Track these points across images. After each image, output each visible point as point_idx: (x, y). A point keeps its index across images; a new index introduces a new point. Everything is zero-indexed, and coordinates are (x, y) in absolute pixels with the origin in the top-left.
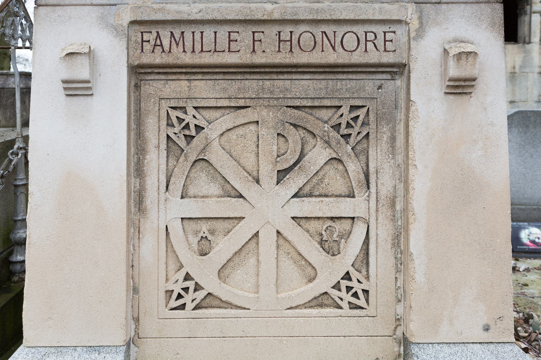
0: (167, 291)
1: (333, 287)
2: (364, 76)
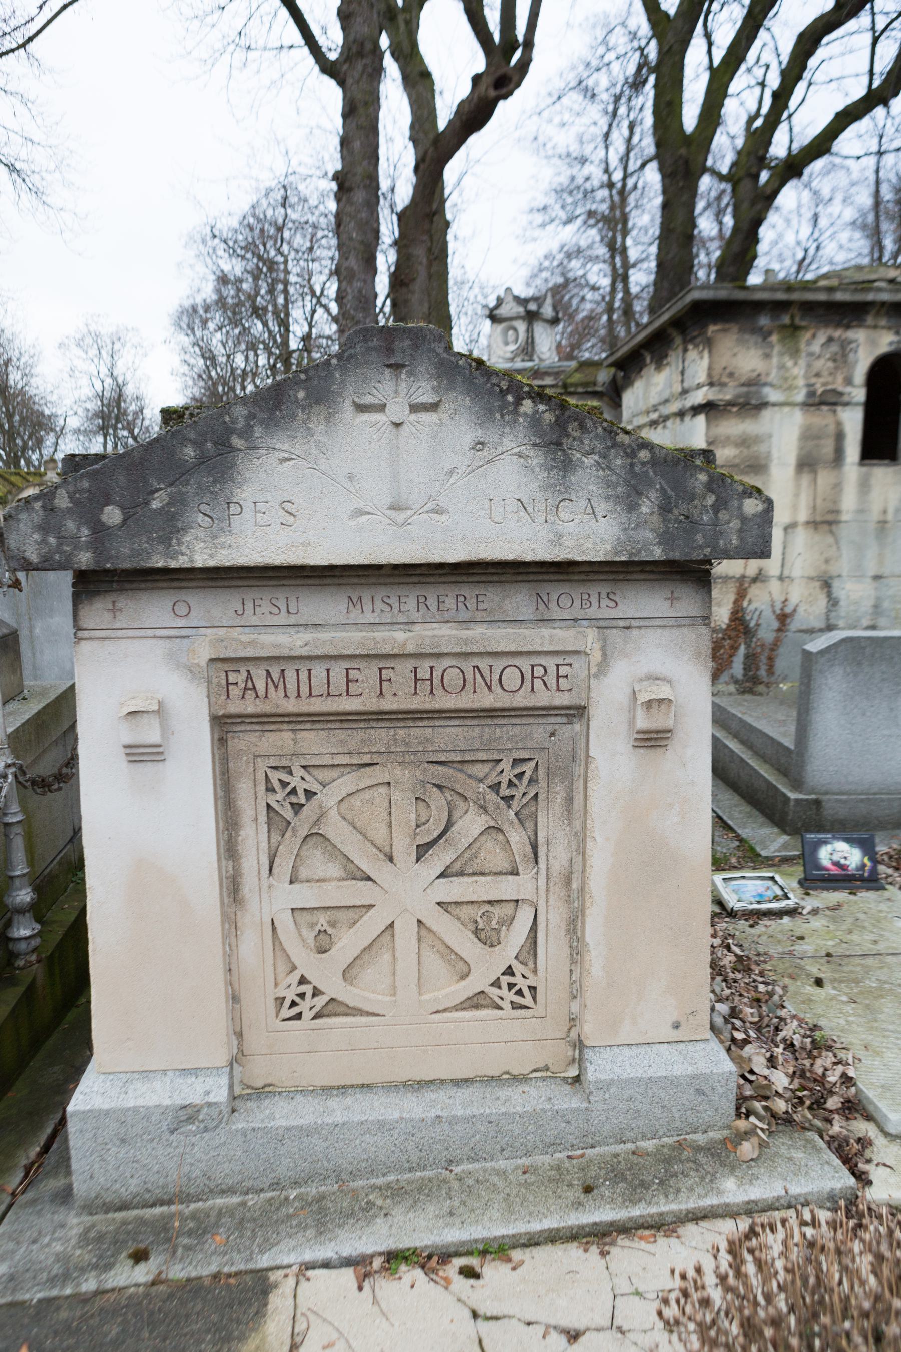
0: (276, 999)
1: (492, 985)
2: (531, 720)
